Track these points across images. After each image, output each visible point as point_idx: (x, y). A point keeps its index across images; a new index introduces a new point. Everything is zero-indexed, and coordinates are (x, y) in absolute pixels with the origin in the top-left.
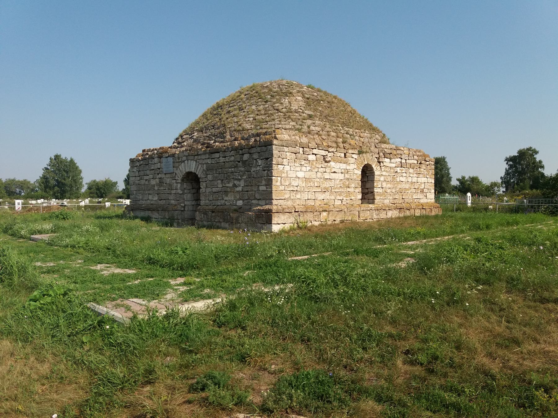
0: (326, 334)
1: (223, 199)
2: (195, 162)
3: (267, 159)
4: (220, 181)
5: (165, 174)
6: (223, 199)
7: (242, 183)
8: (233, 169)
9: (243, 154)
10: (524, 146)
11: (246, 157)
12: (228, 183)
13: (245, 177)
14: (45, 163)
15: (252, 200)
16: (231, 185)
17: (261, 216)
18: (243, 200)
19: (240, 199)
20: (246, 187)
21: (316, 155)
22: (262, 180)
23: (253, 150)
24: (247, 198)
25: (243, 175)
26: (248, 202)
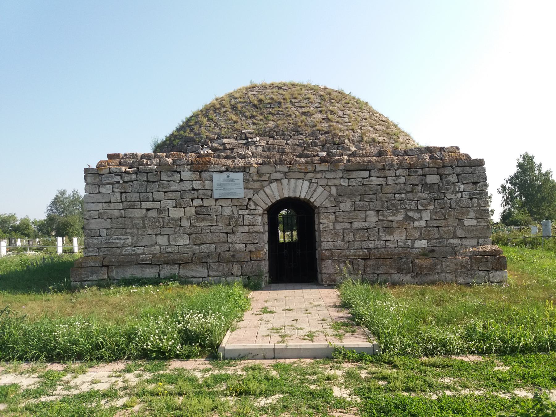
0: (173, 339)
1: (379, 239)
2: (306, 184)
3: (475, 183)
4: (373, 213)
5: (216, 200)
6: (379, 239)
7: (426, 216)
8: (403, 195)
9: (425, 175)
10: (52, 198)
11: (433, 179)
12: (394, 215)
13: (432, 207)
14: (117, 153)
15: (448, 239)
16: (400, 217)
17: (484, 260)
18: (429, 240)
19: (421, 238)
20: (435, 221)
21: (193, 189)
22: (469, 211)
23: (447, 171)
24: (437, 236)
25: (429, 204)
26: (440, 243)
